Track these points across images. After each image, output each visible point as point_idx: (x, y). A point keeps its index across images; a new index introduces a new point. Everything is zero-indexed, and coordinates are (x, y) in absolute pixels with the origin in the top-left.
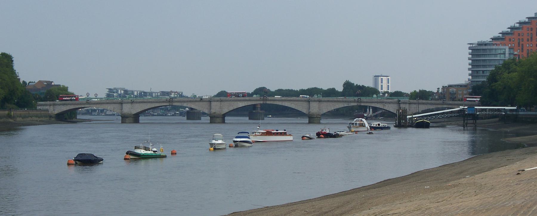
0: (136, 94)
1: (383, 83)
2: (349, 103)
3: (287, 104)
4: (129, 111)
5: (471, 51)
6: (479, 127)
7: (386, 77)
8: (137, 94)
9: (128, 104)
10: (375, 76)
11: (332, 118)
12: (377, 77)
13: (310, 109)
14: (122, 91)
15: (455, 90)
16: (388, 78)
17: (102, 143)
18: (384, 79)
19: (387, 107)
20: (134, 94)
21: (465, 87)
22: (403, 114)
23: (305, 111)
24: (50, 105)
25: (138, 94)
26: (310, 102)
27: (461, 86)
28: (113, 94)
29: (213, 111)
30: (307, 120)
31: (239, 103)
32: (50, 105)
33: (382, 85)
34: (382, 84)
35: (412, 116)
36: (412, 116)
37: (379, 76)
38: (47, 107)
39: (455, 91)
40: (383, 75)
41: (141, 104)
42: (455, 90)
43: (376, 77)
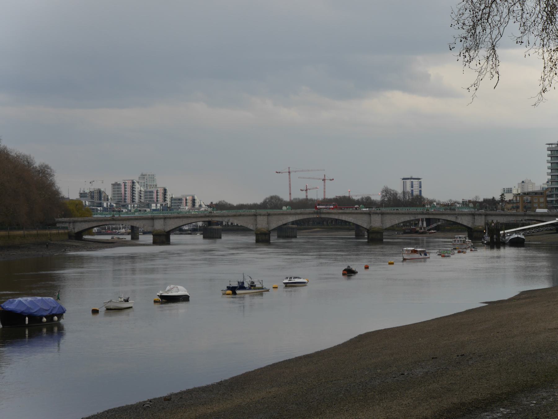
0: (106, 207)
1: (414, 187)
2: (416, 216)
3: (344, 218)
4: (162, 228)
5: (550, 152)
6: (4, 294)
7: (417, 180)
8: (107, 206)
9: (161, 220)
10: (404, 179)
11: (101, 239)
12: (405, 180)
13: (371, 223)
14: (86, 202)
15: (530, 198)
16: (419, 180)
17: (283, 258)
18: (415, 182)
19: (459, 219)
20: (103, 206)
21: (541, 195)
22: (498, 228)
23: (251, 227)
24: (69, 222)
25: (109, 206)
26: (372, 215)
27: (536, 193)
28: (97, 209)
29: (259, 226)
30: (252, 239)
31: (288, 217)
32: (70, 223)
33: (413, 190)
34: (412, 189)
35: (504, 232)
36: (504, 232)
37: (408, 179)
38: (67, 225)
39: (530, 199)
40: (413, 177)
41: (176, 220)
42: (529, 198)
43: (404, 180)
